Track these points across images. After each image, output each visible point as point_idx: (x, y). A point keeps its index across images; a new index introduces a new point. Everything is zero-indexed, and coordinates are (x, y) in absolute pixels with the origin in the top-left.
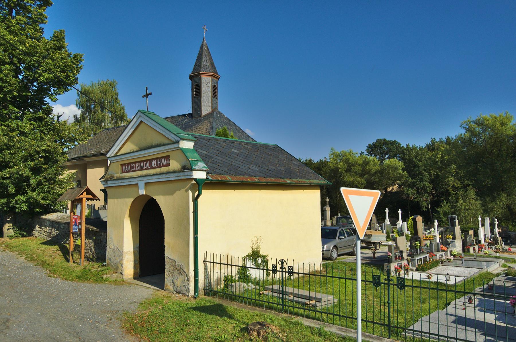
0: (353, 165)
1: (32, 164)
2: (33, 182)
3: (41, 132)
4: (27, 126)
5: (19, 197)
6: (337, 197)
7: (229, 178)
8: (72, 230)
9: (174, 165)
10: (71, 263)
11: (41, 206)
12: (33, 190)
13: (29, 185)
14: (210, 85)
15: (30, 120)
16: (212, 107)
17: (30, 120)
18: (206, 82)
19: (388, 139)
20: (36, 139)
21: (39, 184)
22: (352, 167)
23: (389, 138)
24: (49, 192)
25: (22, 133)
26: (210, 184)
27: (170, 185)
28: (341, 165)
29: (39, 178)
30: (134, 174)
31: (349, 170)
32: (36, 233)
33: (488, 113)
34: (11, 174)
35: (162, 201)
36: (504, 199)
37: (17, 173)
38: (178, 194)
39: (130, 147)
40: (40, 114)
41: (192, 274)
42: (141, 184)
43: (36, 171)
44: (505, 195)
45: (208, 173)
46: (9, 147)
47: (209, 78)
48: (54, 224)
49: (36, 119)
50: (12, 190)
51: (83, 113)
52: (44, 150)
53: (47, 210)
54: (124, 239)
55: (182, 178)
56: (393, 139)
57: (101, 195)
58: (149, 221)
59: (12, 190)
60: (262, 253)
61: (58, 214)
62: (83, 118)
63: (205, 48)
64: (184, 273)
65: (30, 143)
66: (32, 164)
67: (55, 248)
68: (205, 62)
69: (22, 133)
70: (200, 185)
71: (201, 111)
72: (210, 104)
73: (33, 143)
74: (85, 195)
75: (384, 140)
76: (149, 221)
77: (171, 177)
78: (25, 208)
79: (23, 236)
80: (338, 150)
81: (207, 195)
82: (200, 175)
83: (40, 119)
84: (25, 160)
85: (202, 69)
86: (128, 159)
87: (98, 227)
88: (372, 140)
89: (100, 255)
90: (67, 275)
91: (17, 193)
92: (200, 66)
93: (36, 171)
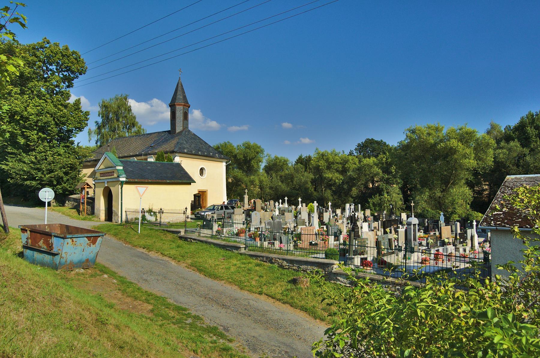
0: (333, 163)
1: (64, 170)
2: (65, 179)
3: (69, 153)
4: (62, 151)
5: (58, 186)
6: (322, 190)
7: (136, 180)
8: (81, 201)
9: (115, 175)
10: (81, 216)
11: (69, 191)
12: (65, 183)
13: (63, 181)
14: (182, 112)
15: (63, 147)
16: (183, 127)
17: (63, 147)
18: (179, 110)
19: (376, 139)
20: (66, 157)
21: (68, 180)
22: (332, 165)
23: (377, 138)
24: (72, 184)
25: (59, 155)
26: (127, 183)
27: (115, 183)
28: (322, 163)
29: (68, 177)
30: (104, 178)
31: (329, 168)
32: (66, 205)
33: (422, 123)
34: (55, 175)
35: (112, 188)
36: (427, 193)
37: (57, 175)
38: (117, 186)
39: (102, 167)
40: (68, 144)
41: (120, 215)
42: (106, 182)
43: (66, 173)
44: (428, 190)
45: (126, 178)
46: (54, 163)
47: (182, 107)
48: (75, 200)
49: (65, 146)
50: (55, 183)
51: (103, 122)
52: (70, 164)
53: (72, 193)
54: (101, 204)
55: (117, 181)
56: (379, 140)
57: (93, 186)
58: (109, 197)
59: (55, 183)
60: (153, 210)
61: (77, 195)
62: (104, 125)
63: (180, 85)
64: (118, 215)
65: (64, 160)
66: (64, 170)
67: (75, 210)
68: (180, 96)
69: (59, 155)
70: (122, 183)
71: (175, 129)
72: (182, 125)
73: (65, 159)
74: (86, 186)
75: (372, 139)
76: (109, 197)
77: (114, 180)
78: (61, 192)
79: (60, 206)
80: (322, 150)
81: (125, 186)
82: (123, 179)
83: (68, 147)
84: (61, 168)
85: (177, 101)
86: (102, 171)
87: (91, 201)
88: (362, 140)
89: (92, 212)
90: (78, 219)
91: (58, 184)
92: (175, 99)
93: (66, 173)
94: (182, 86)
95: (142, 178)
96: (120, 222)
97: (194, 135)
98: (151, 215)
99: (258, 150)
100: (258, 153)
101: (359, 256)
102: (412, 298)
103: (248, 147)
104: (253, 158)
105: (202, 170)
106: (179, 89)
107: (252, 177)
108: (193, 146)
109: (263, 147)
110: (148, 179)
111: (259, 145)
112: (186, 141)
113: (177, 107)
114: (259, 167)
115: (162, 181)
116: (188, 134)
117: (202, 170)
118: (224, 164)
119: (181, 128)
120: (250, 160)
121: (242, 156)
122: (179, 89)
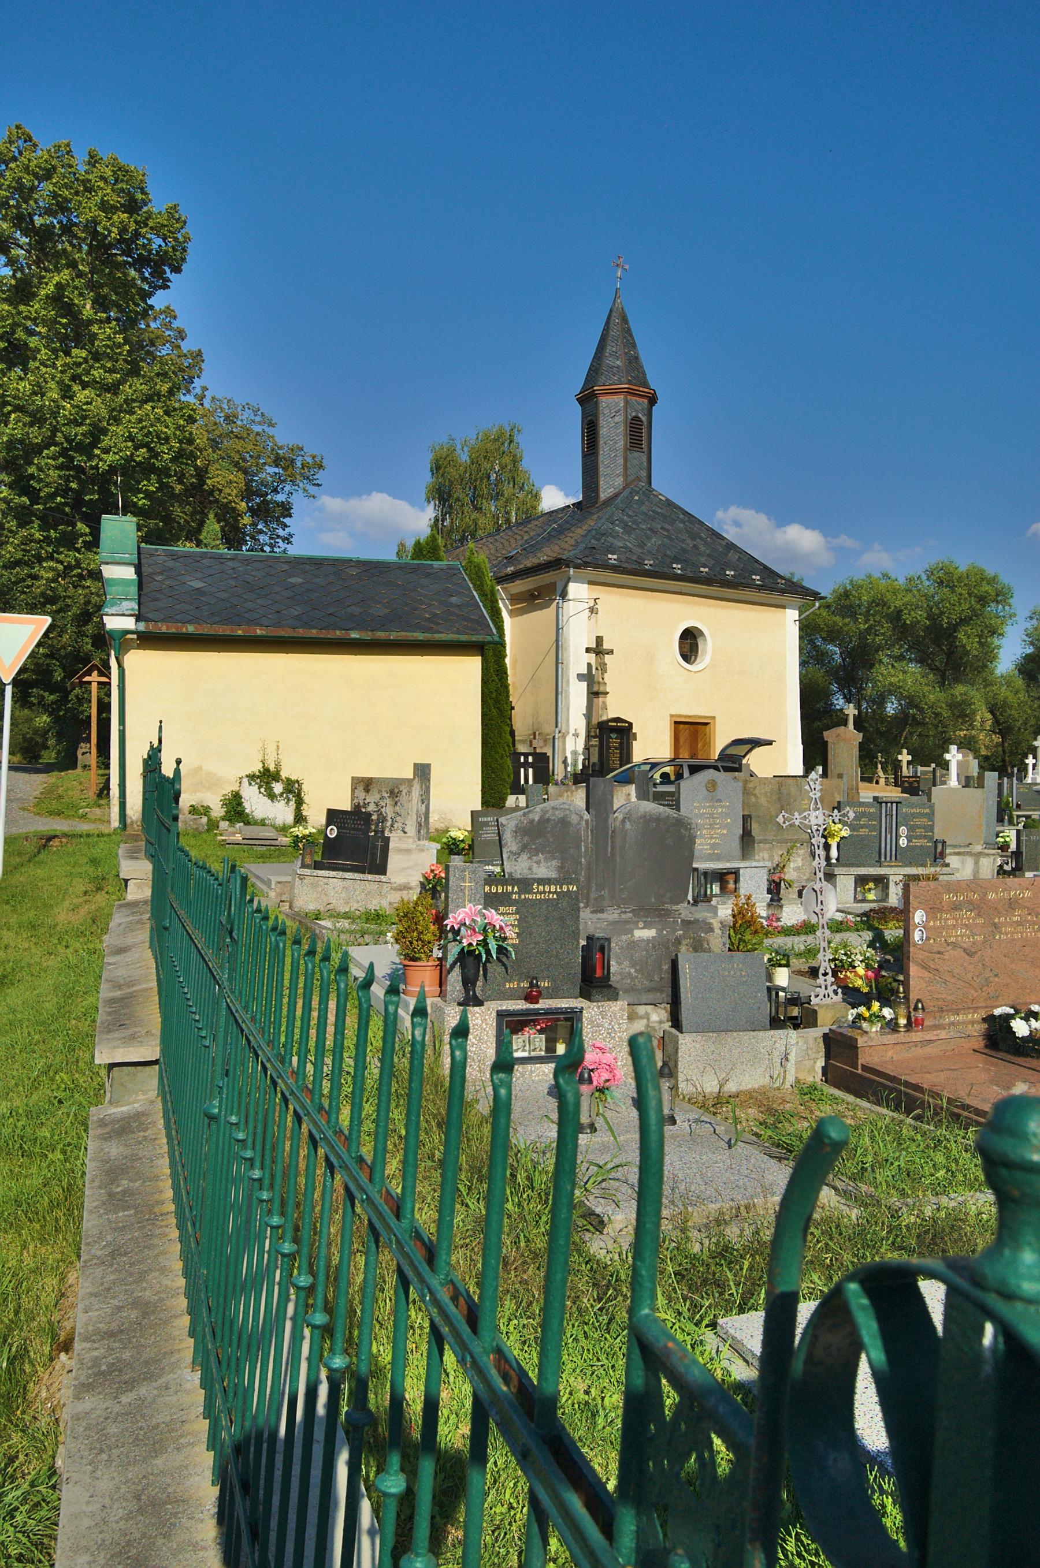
16: (626, 475)
26: (149, 640)
45: (139, 618)
72: (620, 470)
94: (624, 320)
95: (227, 621)
96: (115, 823)
97: (669, 503)
98: (272, 796)
99: (986, 587)
100: (983, 600)
101: (889, 905)
102: (128, 1364)
103: (946, 579)
104: (965, 621)
105: (690, 643)
106: (616, 332)
107: (960, 689)
108: (654, 542)
109: (1005, 579)
110: (252, 622)
111: (990, 572)
112: (625, 527)
113: (604, 401)
114: (989, 656)
115: (324, 634)
116: (641, 502)
117: (690, 643)
118: (792, 615)
119: (619, 481)
120: (955, 628)
121: (920, 615)
122: (616, 332)
